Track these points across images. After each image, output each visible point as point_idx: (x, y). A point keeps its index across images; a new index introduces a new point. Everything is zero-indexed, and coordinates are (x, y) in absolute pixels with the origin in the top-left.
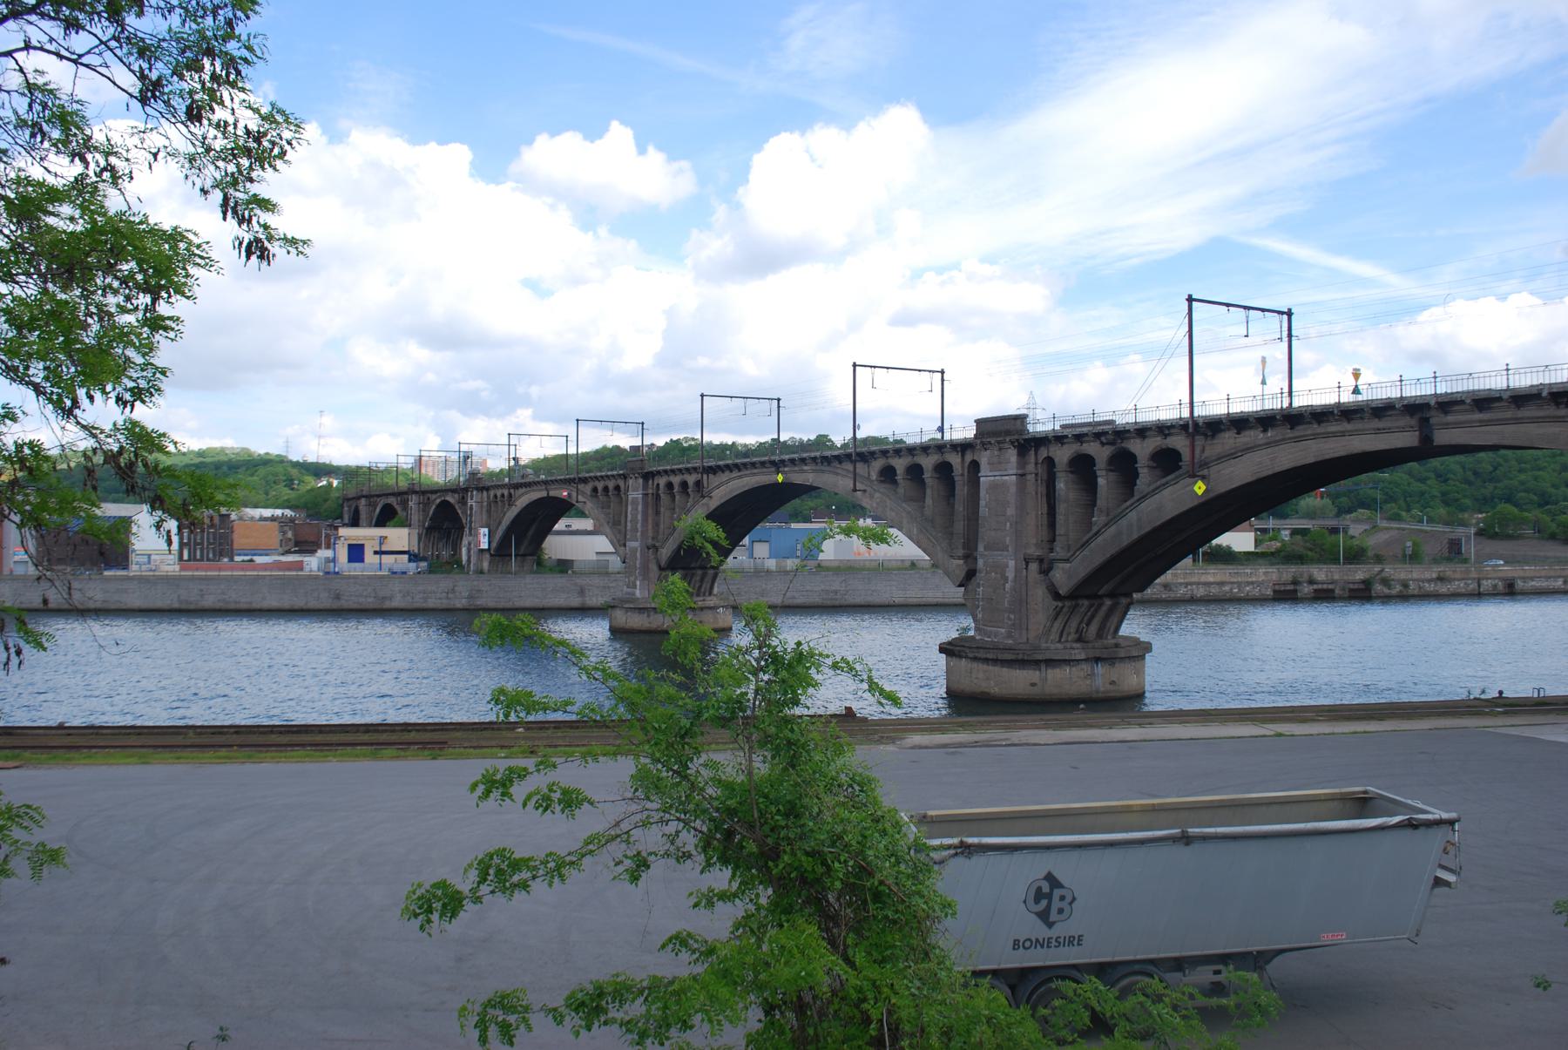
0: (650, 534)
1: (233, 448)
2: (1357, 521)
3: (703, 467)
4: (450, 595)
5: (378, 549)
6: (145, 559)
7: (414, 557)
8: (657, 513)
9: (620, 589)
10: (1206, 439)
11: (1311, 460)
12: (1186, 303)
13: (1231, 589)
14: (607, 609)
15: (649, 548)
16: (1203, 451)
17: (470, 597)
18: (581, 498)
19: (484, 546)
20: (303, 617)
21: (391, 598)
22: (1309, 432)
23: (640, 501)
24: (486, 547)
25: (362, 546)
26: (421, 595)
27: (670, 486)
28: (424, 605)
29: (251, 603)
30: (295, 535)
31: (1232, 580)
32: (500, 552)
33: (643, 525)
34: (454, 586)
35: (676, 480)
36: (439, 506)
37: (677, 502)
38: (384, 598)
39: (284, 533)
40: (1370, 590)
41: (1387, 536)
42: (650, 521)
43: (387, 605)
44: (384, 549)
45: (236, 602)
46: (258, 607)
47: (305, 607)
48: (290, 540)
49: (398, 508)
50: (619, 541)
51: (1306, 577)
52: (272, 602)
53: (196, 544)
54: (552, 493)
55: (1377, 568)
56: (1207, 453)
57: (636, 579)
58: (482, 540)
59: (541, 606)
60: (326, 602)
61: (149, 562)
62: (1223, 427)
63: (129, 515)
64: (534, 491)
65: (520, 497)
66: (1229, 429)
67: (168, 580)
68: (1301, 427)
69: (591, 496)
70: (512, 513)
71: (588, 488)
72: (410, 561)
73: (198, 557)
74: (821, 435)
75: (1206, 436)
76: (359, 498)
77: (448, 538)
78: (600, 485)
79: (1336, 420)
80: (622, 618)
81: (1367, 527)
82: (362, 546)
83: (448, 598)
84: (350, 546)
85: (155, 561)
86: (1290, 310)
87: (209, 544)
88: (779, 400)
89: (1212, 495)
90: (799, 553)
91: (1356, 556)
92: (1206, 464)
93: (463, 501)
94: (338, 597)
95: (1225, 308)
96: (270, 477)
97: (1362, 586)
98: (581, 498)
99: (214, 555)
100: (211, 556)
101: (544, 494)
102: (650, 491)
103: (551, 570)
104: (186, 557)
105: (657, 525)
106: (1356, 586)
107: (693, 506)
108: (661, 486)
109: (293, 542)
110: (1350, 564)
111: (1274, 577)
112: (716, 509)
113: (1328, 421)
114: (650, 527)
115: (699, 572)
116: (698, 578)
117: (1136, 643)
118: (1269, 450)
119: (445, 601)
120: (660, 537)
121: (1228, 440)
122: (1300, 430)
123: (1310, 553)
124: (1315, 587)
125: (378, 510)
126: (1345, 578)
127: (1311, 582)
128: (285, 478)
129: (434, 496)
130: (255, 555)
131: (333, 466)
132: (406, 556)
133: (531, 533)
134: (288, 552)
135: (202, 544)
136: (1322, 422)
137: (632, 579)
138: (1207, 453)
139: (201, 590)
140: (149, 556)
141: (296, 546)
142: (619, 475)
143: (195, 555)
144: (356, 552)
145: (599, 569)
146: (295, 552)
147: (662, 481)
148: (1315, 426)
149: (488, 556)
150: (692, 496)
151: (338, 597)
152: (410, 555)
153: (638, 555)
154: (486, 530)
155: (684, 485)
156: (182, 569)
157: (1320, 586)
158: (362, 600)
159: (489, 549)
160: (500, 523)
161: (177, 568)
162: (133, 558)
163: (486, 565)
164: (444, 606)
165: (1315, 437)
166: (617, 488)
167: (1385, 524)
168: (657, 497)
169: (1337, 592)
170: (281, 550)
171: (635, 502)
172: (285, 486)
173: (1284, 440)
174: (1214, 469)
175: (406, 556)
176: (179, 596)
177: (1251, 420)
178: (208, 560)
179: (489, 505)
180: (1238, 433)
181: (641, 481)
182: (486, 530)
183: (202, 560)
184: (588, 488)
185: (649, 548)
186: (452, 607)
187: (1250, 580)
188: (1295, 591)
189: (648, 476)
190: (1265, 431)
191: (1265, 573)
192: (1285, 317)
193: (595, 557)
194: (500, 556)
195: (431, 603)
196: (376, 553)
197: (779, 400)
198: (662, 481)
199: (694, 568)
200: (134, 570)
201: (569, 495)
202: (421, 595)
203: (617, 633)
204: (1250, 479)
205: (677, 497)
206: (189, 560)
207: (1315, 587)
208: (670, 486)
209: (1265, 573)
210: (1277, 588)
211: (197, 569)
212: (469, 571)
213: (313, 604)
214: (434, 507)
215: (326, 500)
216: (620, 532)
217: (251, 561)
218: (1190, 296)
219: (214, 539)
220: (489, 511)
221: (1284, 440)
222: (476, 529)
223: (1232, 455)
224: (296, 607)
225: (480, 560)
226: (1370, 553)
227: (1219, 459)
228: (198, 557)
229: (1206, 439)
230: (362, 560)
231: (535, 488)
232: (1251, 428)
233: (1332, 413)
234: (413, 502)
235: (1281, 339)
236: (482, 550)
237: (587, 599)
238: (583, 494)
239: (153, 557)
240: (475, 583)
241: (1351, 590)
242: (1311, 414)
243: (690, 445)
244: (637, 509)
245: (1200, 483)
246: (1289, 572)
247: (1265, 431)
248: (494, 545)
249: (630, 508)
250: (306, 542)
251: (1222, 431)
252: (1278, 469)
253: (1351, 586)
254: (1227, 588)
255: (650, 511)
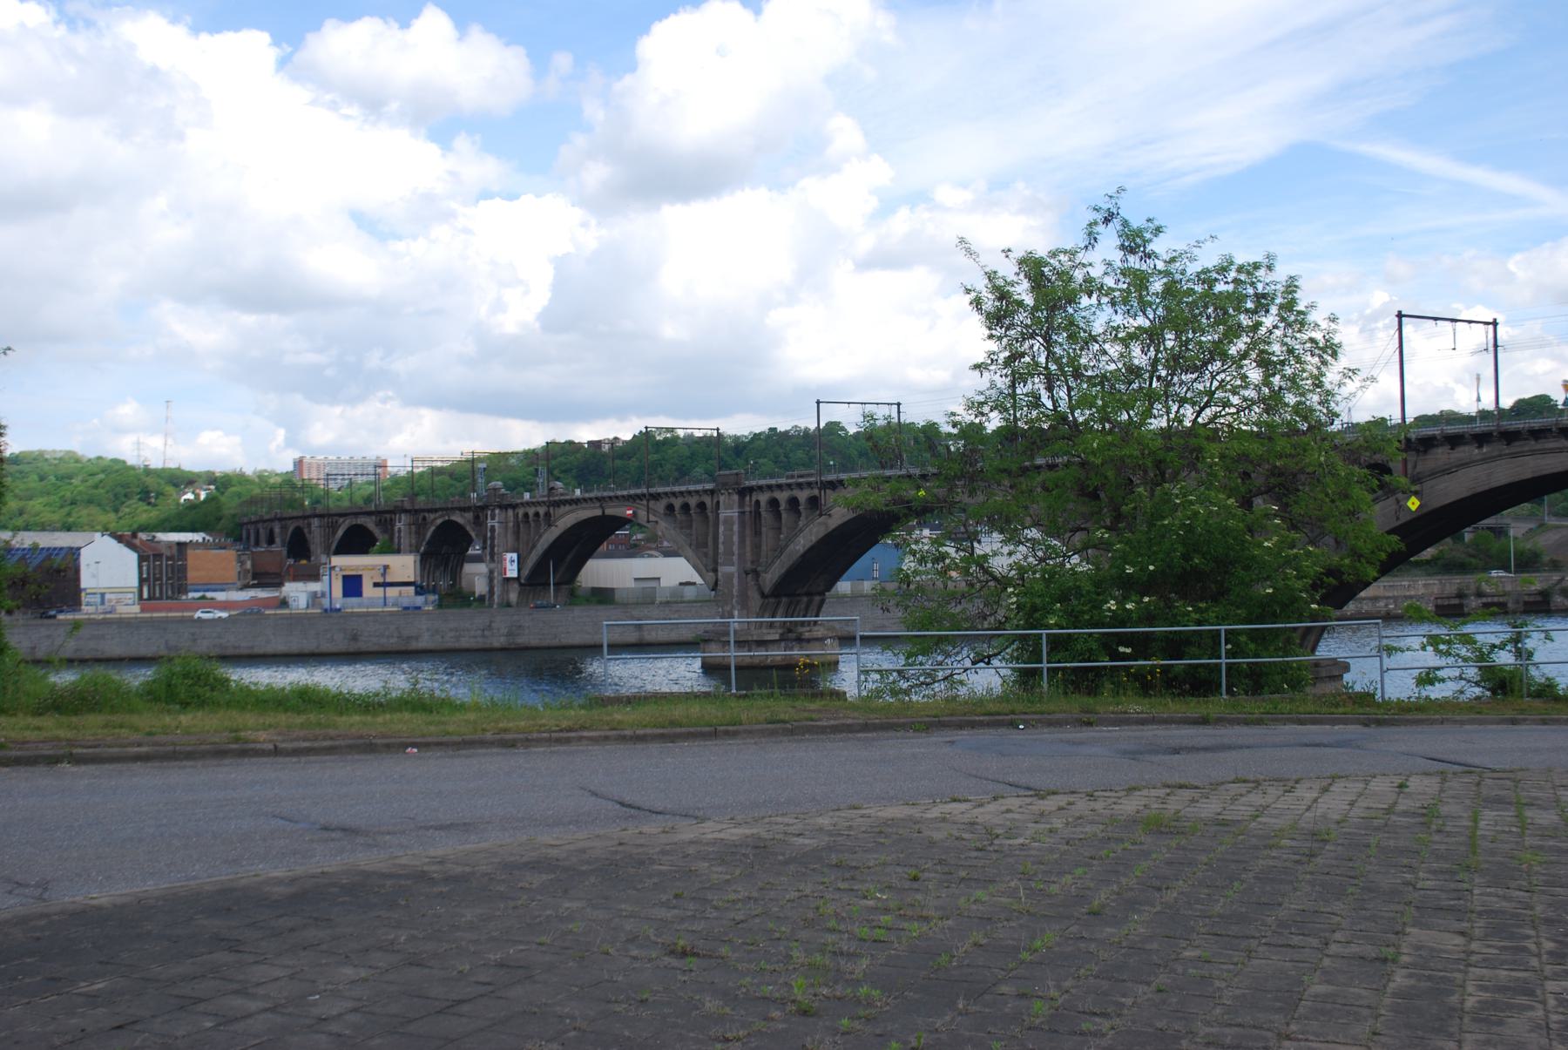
0: (749, 556)
1: (54, 451)
2: (1517, 518)
3: (822, 482)
4: (486, 633)
5: (381, 580)
6: (98, 599)
7: (420, 590)
8: (757, 533)
9: (708, 620)
10: (1418, 456)
11: (1528, 475)
12: (1396, 319)
13: (1386, 605)
14: (698, 644)
15: (747, 574)
16: (1415, 467)
17: (509, 634)
18: (652, 518)
19: (512, 571)
20: (679, 651)
21: (417, 638)
22: (1526, 448)
23: (736, 520)
24: (515, 575)
25: (359, 578)
26: (452, 634)
27: (774, 503)
28: (457, 645)
29: (252, 647)
30: (253, 565)
31: (1387, 594)
32: (533, 581)
33: (739, 548)
34: (491, 622)
35: (782, 496)
36: (439, 527)
37: (783, 521)
38: (409, 638)
39: (242, 563)
40: (1548, 603)
41: (1557, 537)
42: (748, 543)
43: (414, 645)
44: (388, 580)
45: (235, 648)
46: (261, 651)
47: (317, 651)
48: (249, 571)
49: (377, 531)
50: (706, 566)
51: (1473, 588)
52: (279, 646)
53: (156, 580)
54: (609, 512)
55: (1556, 577)
56: (1418, 470)
57: (733, 608)
58: (508, 566)
59: (592, 643)
60: (341, 645)
61: (103, 603)
62: (1436, 443)
63: (75, 545)
64: (584, 509)
65: (562, 516)
66: (1442, 445)
67: (125, 624)
68: (1517, 443)
69: (665, 514)
70: (550, 536)
71: (660, 506)
72: (417, 593)
73: (157, 595)
74: (832, 423)
75: (1418, 451)
76: (271, 520)
77: (446, 565)
78: (677, 503)
79: (1554, 437)
80: (715, 653)
81: (1532, 526)
82: (359, 578)
83: (483, 636)
84: (345, 578)
85: (110, 601)
86: (1495, 320)
87: (168, 579)
88: (899, 404)
89: (1425, 510)
90: (876, 574)
91: (1528, 562)
92: (1419, 479)
93: (478, 521)
94: (355, 638)
95: (1434, 322)
96: (119, 489)
97: (1539, 598)
98: (652, 518)
99: (173, 593)
100: (170, 593)
101: (598, 512)
102: (747, 509)
103: (588, 601)
104: (145, 595)
105: (757, 547)
106: (1532, 599)
107: (807, 525)
108: (763, 504)
109: (250, 575)
110: (1522, 572)
111: (1436, 590)
112: (834, 530)
113: (1545, 438)
114: (748, 549)
115: (805, 599)
116: (803, 606)
117: (1334, 662)
118: (1485, 466)
119: (480, 640)
120: (763, 560)
121: (1441, 455)
122: (1517, 447)
123: (1473, 560)
124: (1484, 600)
125: (340, 533)
126: (1519, 589)
127: (1480, 594)
128: (139, 490)
129: (432, 516)
130: (208, 590)
131: (183, 471)
132: (411, 589)
133: (569, 557)
134: (245, 587)
135: (160, 579)
136: (1540, 438)
137: (728, 608)
138: (1418, 470)
139: (193, 634)
140: (103, 595)
141: (254, 579)
142: (705, 491)
143: (154, 594)
144: (352, 585)
145: (675, 601)
146: (254, 586)
147: (764, 498)
148: (1533, 442)
149: (516, 585)
150: (803, 515)
151: (355, 638)
152: (416, 587)
153: (735, 581)
154: (515, 556)
155: (793, 502)
156: (143, 610)
157: (1490, 600)
158: (383, 641)
159: (518, 579)
160: (534, 546)
161: (136, 609)
162: (84, 598)
163: (513, 597)
164: (480, 646)
165: (1533, 453)
166: (702, 506)
167: (1553, 521)
168: (757, 514)
169: (1510, 605)
170: (239, 584)
171: (728, 521)
172: (140, 499)
173: (1500, 456)
174: (1427, 485)
175: (411, 589)
176: (167, 642)
177: (1467, 436)
178: (168, 598)
179: (517, 525)
180: (1452, 449)
181: (736, 497)
182: (515, 556)
183: (161, 598)
184: (660, 506)
185: (747, 574)
186: (487, 646)
187: (1408, 594)
188: (1461, 606)
189: (744, 492)
190: (1480, 446)
191: (1425, 585)
192: (1491, 327)
193: (632, 584)
194: (530, 585)
195: (465, 643)
196: (376, 585)
197: (899, 404)
198: (764, 498)
199: (799, 595)
200: (88, 610)
201: (635, 514)
202: (452, 634)
203: (709, 669)
204: (1465, 494)
205: (784, 516)
206: (150, 598)
207: (1484, 600)
208: (774, 503)
209: (1425, 585)
210: (1440, 602)
211: (170, 610)
212: (491, 606)
213: (326, 647)
214: (433, 528)
215: (219, 519)
216: (706, 555)
217: (203, 597)
218: (1400, 312)
219: (173, 572)
220: (517, 533)
221: (1500, 456)
222: (500, 555)
223: (1447, 471)
224: (306, 651)
225: (506, 592)
226: (1546, 559)
227: (1433, 474)
228: (157, 595)
229: (1418, 456)
230: (360, 594)
231: (584, 505)
232: (1465, 444)
233: (1550, 430)
234: (401, 523)
235: (1486, 350)
236: (509, 579)
237: (645, 633)
238: (655, 513)
239: (107, 597)
240: (515, 618)
241: (1526, 603)
242: (1529, 431)
243: (666, 439)
244: (732, 530)
245: (1413, 499)
246: (1452, 583)
247: (1480, 446)
248: (526, 572)
249: (721, 529)
250: (267, 574)
251: (1434, 446)
252: (1495, 484)
253: (1526, 598)
254: (1382, 604)
255: (748, 532)
